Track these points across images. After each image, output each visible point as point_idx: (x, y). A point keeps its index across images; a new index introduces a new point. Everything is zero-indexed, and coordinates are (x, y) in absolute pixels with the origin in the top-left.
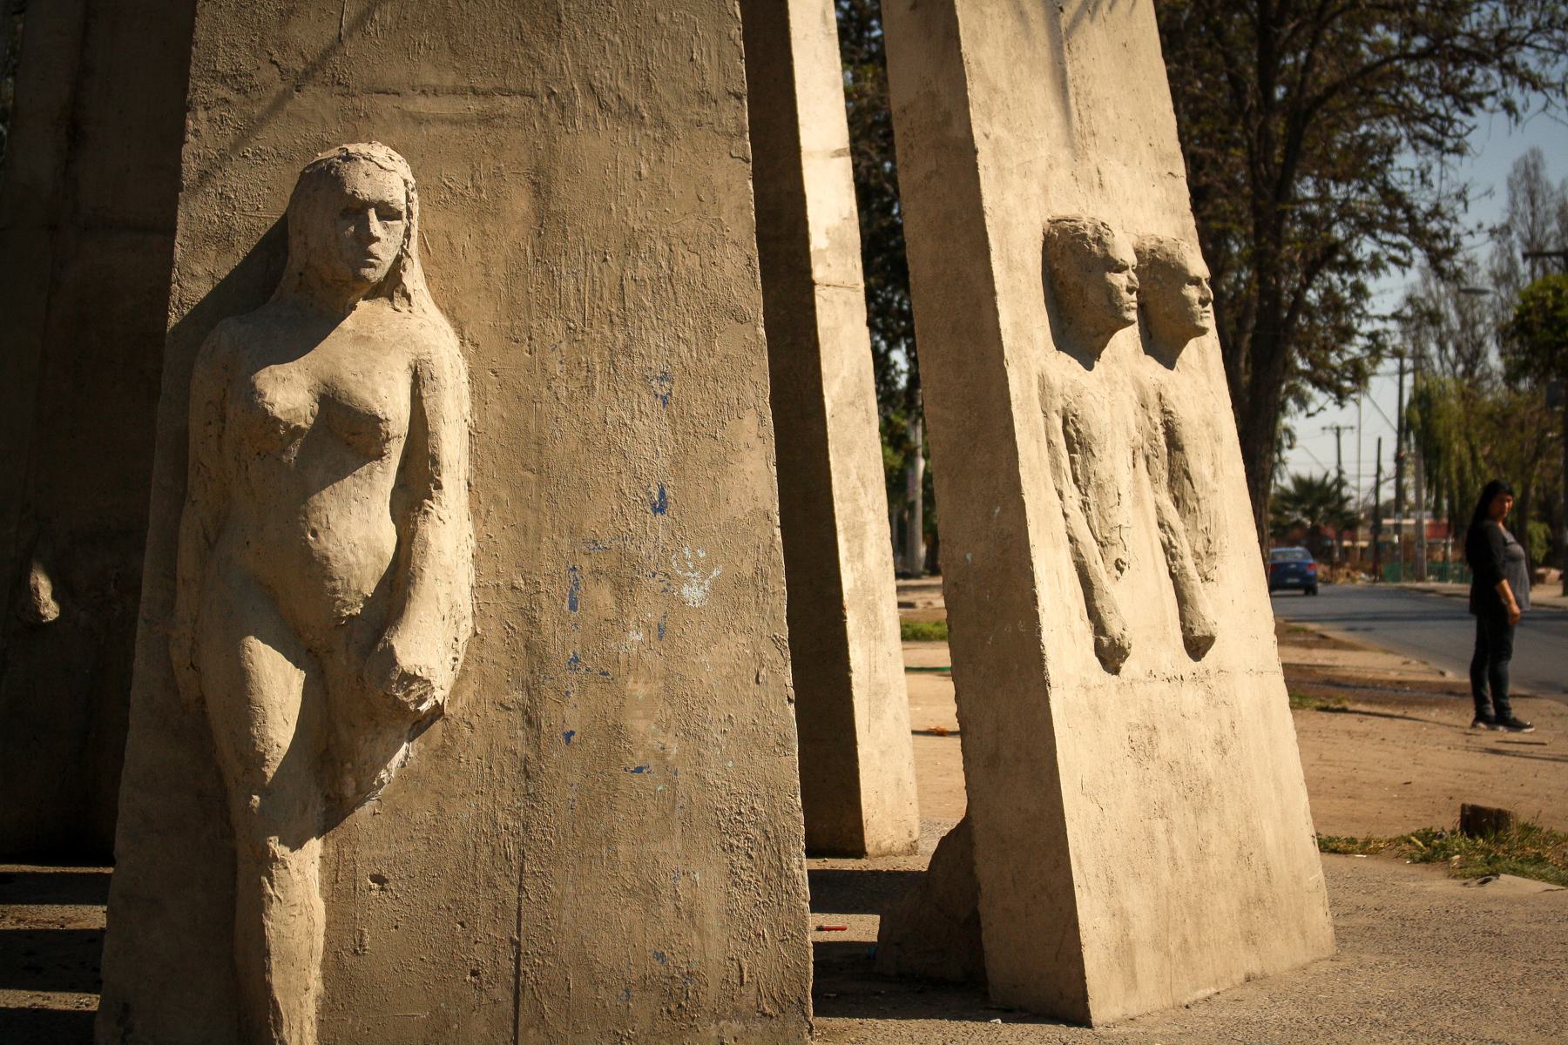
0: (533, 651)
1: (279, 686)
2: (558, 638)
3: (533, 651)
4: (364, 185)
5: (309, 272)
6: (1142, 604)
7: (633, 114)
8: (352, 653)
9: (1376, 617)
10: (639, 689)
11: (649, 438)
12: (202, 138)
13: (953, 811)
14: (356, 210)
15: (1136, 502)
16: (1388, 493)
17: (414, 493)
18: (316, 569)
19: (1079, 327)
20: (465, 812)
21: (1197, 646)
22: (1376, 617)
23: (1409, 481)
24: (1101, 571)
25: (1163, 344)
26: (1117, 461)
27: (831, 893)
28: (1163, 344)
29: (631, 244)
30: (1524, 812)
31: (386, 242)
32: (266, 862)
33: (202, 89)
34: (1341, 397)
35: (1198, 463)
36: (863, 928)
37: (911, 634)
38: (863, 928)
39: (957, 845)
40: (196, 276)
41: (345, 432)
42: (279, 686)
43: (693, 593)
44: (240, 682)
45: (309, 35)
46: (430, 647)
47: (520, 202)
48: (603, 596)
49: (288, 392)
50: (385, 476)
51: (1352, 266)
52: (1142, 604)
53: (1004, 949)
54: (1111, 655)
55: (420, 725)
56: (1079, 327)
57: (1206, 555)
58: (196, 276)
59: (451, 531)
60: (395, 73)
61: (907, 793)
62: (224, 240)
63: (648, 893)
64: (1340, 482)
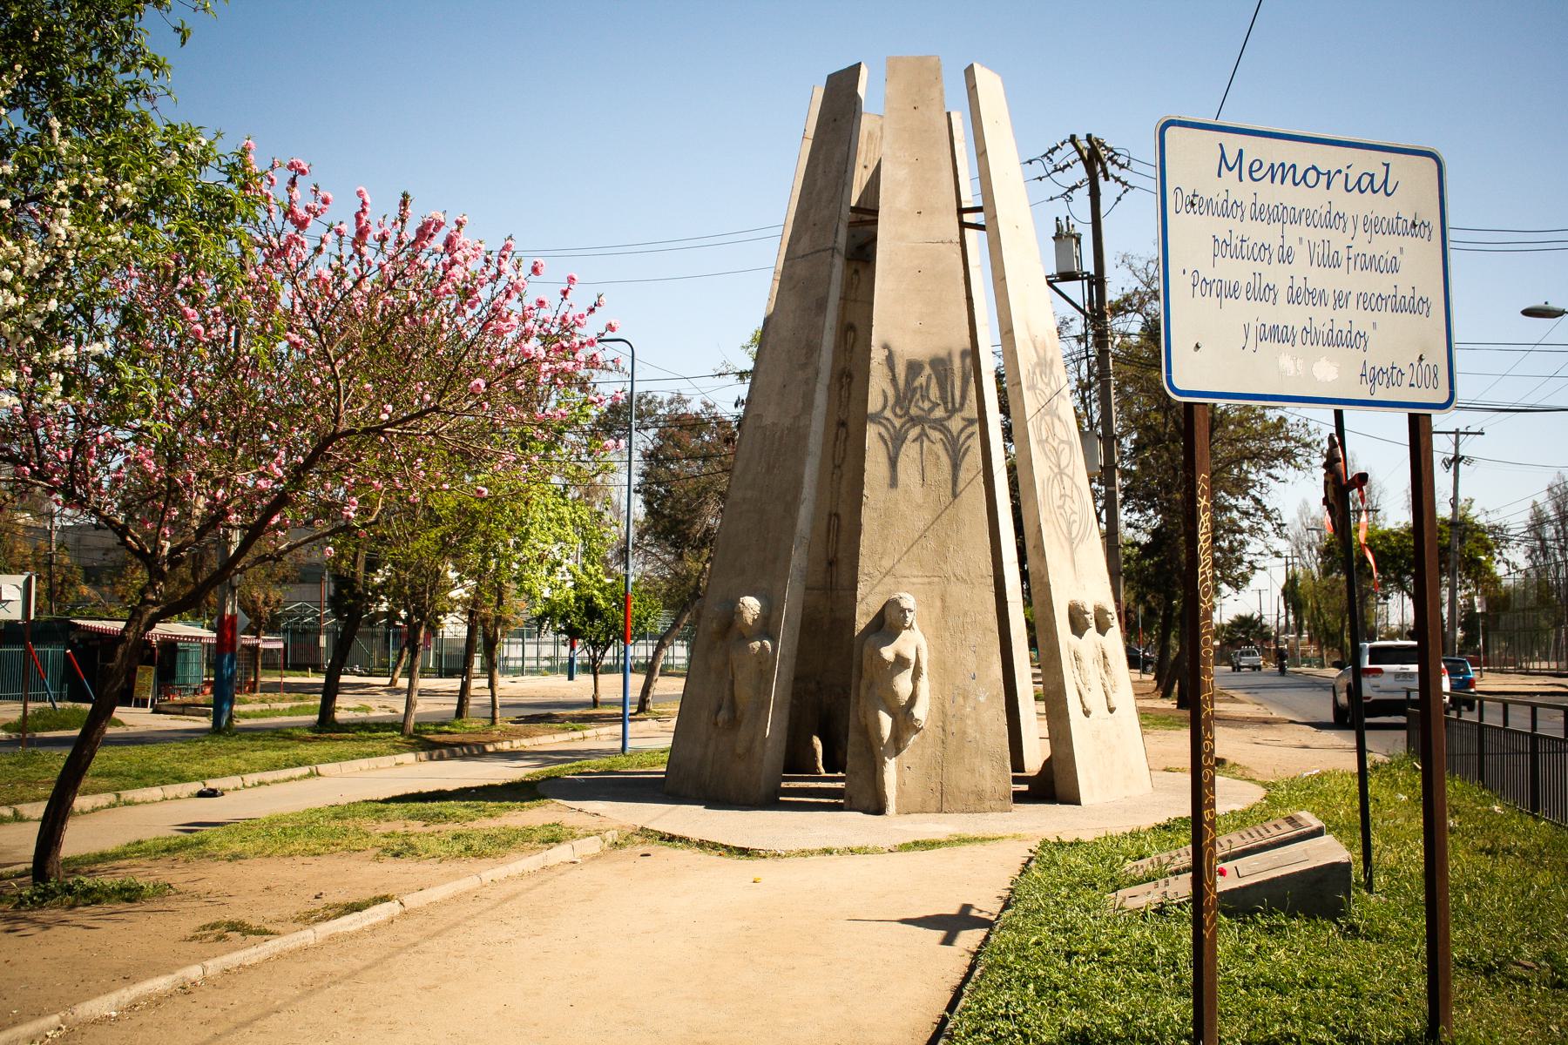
0: (944, 713)
1: (886, 721)
2: (950, 710)
3: (944, 713)
4: (904, 604)
5: (888, 623)
6: (1095, 701)
7: (965, 581)
8: (904, 717)
9: (1265, 687)
10: (969, 722)
11: (971, 661)
12: (861, 590)
13: (1048, 754)
14: (903, 611)
15: (1093, 671)
16: (1282, 622)
17: (916, 677)
18: (895, 694)
19: (1078, 626)
20: (929, 751)
21: (1111, 710)
22: (1265, 687)
23: (1291, 617)
24: (1084, 692)
25: (1102, 628)
26: (1088, 662)
27: (1016, 780)
28: (1102, 628)
29: (965, 614)
30: (1231, 760)
31: (910, 617)
32: (884, 762)
33: (861, 577)
34: (1238, 588)
35: (1111, 660)
36: (1025, 788)
37: (1037, 699)
38: (1025, 788)
39: (1048, 764)
40: (861, 623)
41: (901, 662)
42: (886, 721)
43: (982, 699)
44: (877, 721)
45: (887, 563)
46: (920, 712)
47: (938, 603)
48: (960, 700)
49: (888, 653)
50: (909, 673)
51: (1241, 532)
52: (1095, 701)
53: (1060, 788)
54: (1087, 713)
55: (918, 730)
56: (1078, 623)
57: (1114, 686)
58: (861, 623)
59: (924, 684)
60: (907, 572)
61: (1035, 755)
62: (868, 614)
63: (972, 771)
64: (1261, 617)
